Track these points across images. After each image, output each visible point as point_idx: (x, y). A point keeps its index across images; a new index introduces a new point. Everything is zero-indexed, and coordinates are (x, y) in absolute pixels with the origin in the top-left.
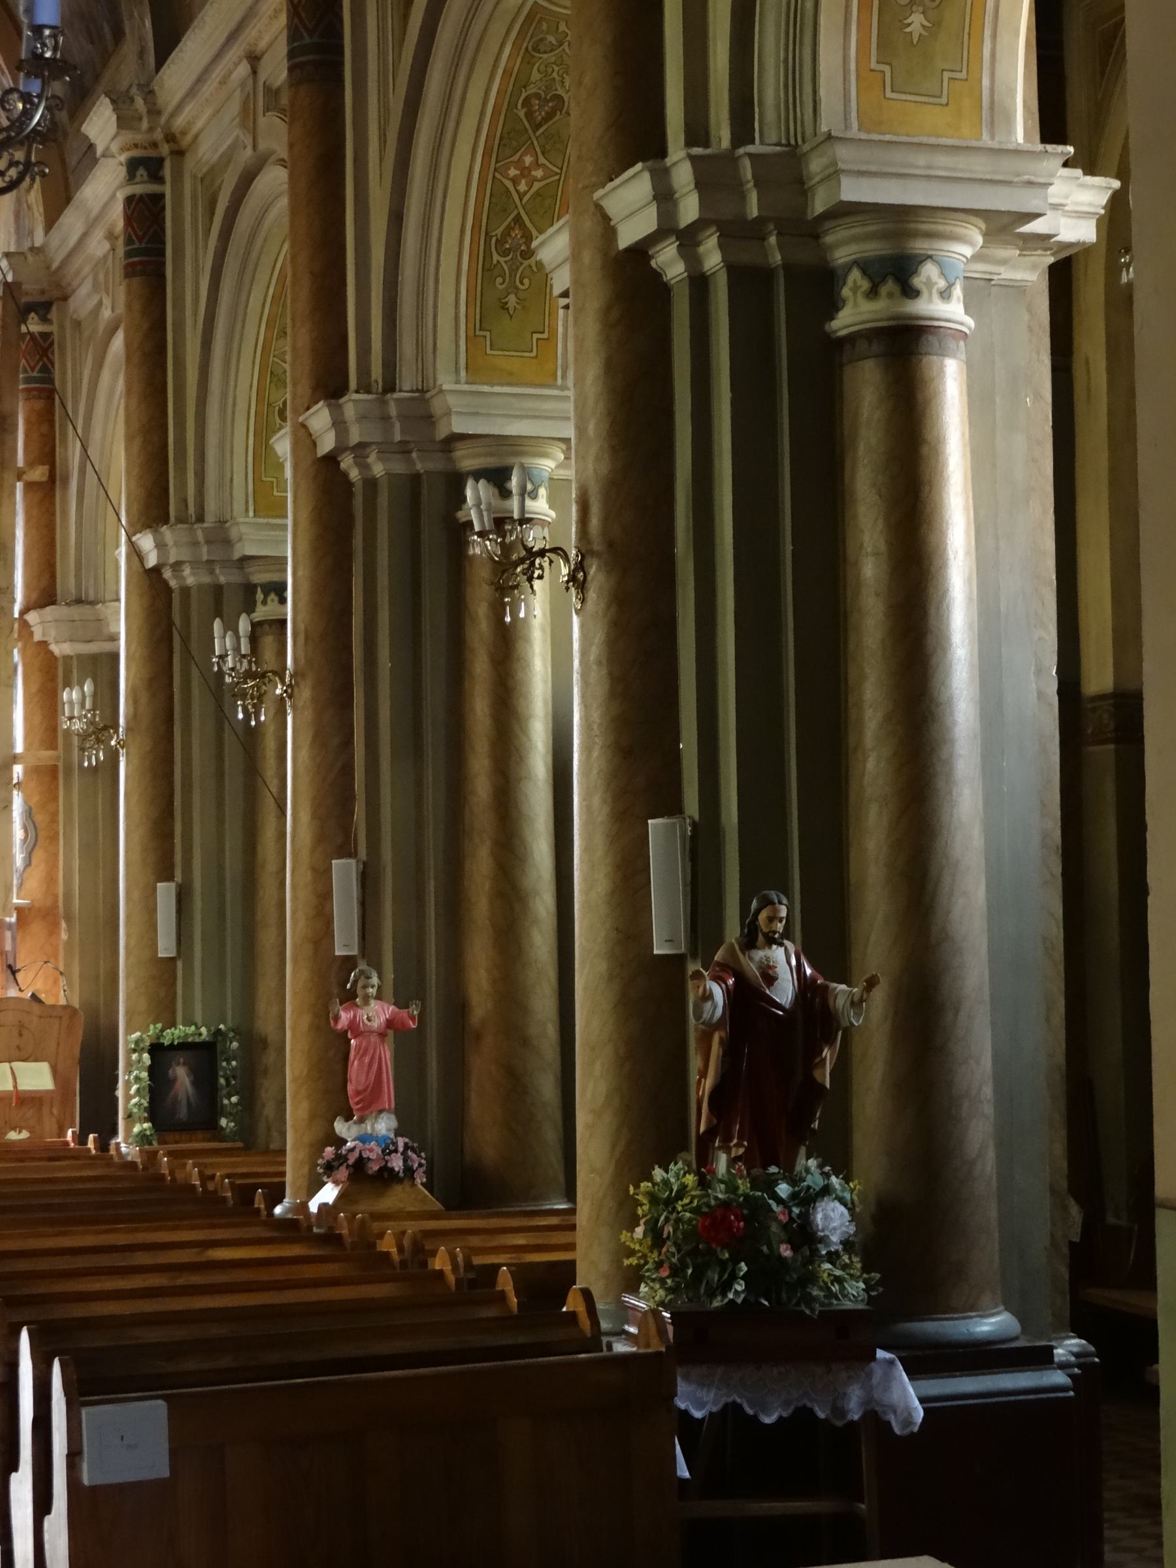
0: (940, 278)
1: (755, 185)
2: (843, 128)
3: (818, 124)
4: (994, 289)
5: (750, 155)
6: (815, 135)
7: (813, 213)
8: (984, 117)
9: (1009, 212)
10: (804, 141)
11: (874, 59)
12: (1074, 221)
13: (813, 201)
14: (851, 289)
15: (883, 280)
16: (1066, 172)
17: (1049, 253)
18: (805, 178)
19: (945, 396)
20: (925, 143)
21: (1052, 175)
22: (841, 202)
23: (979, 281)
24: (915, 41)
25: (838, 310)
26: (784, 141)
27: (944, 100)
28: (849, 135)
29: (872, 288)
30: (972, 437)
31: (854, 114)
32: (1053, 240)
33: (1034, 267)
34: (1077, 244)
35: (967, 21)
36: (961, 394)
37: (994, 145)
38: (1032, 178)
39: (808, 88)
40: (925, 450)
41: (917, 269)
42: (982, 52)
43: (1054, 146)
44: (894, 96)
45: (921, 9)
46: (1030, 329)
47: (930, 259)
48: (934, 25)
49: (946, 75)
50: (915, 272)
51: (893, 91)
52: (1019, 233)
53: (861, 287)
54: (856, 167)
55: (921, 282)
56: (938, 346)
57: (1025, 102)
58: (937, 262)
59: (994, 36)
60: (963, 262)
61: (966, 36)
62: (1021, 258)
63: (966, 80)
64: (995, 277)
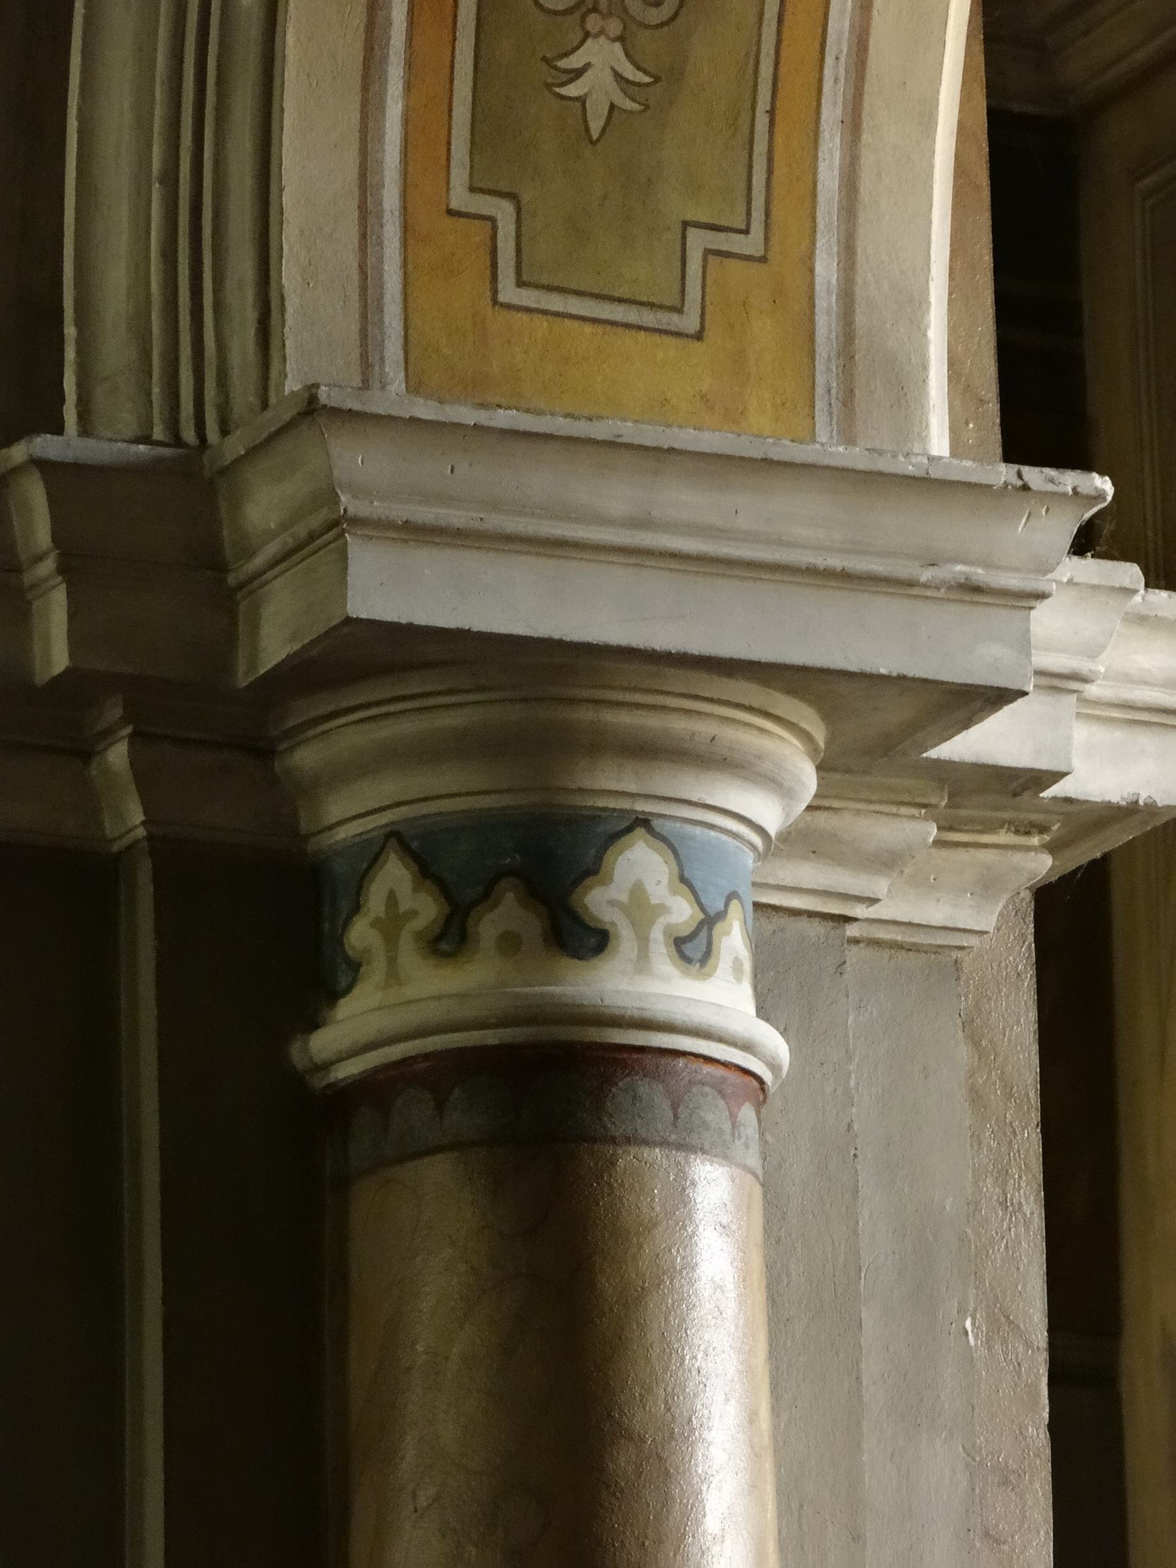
0: (674, 892)
1: (62, 570)
2: (357, 381)
3: (274, 374)
4: (854, 955)
5: (42, 465)
6: (265, 405)
7: (253, 663)
8: (820, 380)
9: (902, 678)
10: (225, 432)
11: (459, 177)
12: (1118, 735)
13: (255, 628)
14: (376, 923)
15: (487, 895)
16: (1090, 569)
17: (1035, 840)
18: (228, 552)
19: (691, 1283)
20: (626, 439)
21: (1044, 568)
22: (348, 621)
23: (803, 923)
24: (595, 127)
25: (334, 996)
26: (158, 433)
27: (690, 321)
28: (378, 404)
29: (448, 921)
30: (781, 1441)
31: (393, 349)
32: (1047, 794)
33: (986, 886)
34: (1129, 811)
35: (768, 47)
36: (744, 1278)
37: (854, 457)
38: (980, 574)
39: (242, 266)
40: (623, 1459)
41: (599, 860)
42: (815, 174)
43: (1051, 472)
44: (528, 297)
45: (614, 27)
46: (976, 1097)
47: (640, 832)
48: (657, 79)
49: (697, 241)
50: (593, 870)
51: (520, 283)
52: (937, 762)
53: (414, 913)
54: (401, 512)
55: (612, 903)
56: (669, 1114)
57: (953, 364)
58: (664, 839)
59: (853, 125)
60: (753, 847)
61: (762, 121)
62: (944, 853)
63: (763, 259)
64: (860, 911)
